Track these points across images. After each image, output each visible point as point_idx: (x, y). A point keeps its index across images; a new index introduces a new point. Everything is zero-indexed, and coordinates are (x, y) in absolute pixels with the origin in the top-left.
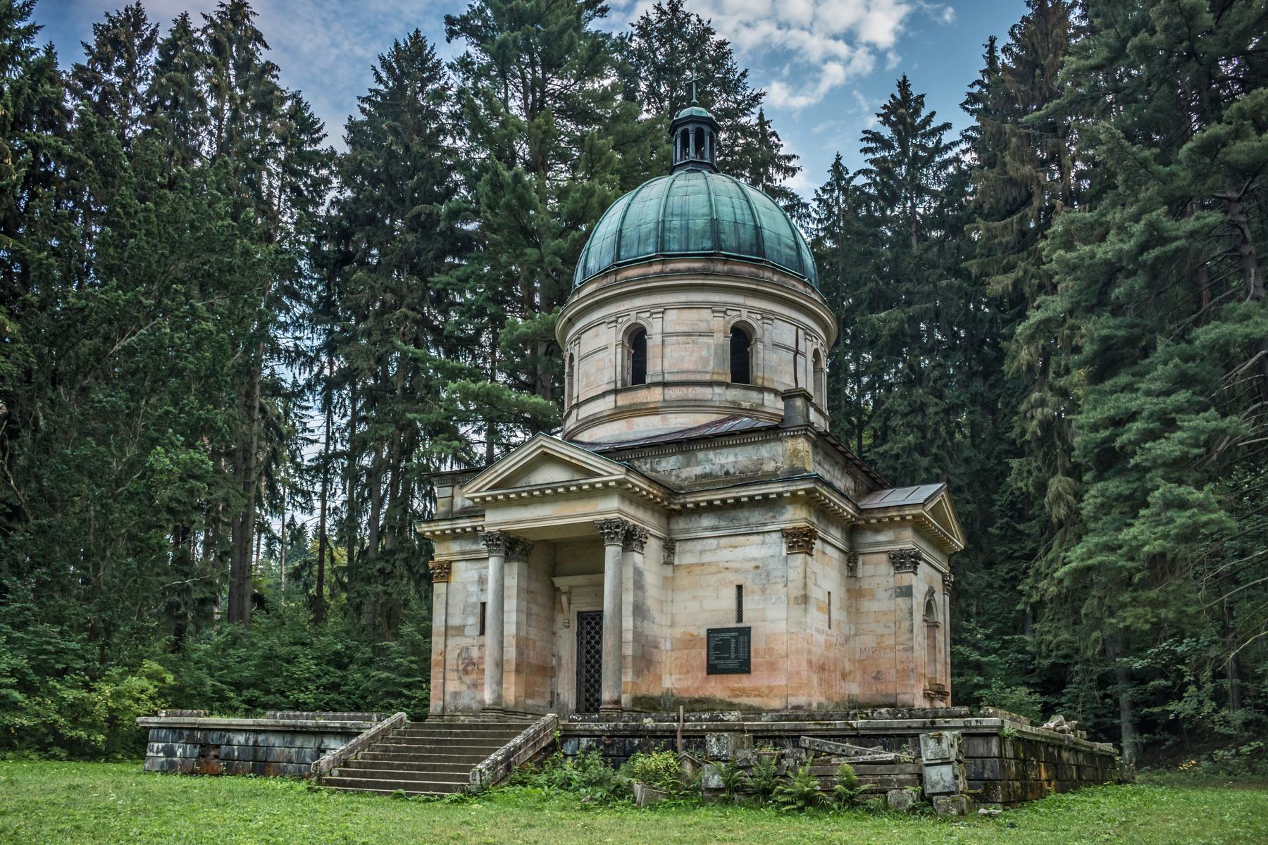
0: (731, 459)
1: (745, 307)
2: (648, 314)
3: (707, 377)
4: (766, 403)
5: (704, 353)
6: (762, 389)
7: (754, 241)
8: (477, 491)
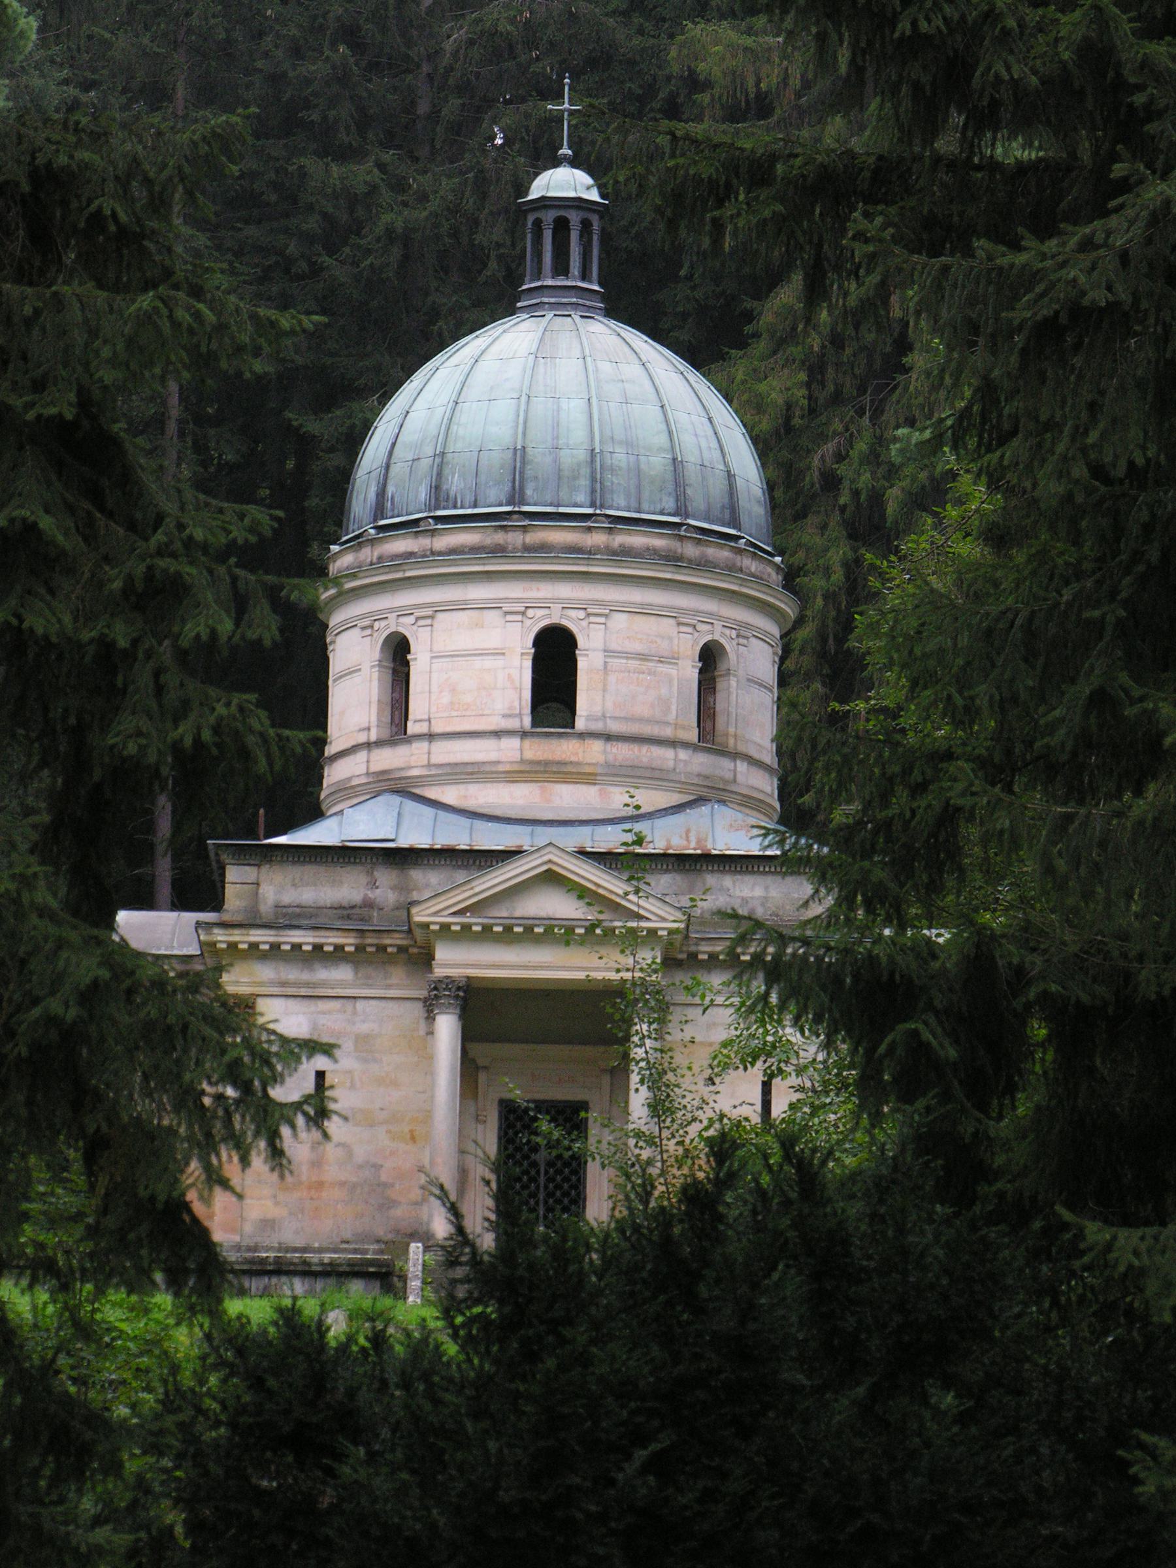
0: (758, 892)
1: (720, 618)
2: (582, 614)
3: (668, 732)
4: (740, 778)
5: (664, 691)
6: (735, 755)
7: (726, 500)
8: (436, 914)
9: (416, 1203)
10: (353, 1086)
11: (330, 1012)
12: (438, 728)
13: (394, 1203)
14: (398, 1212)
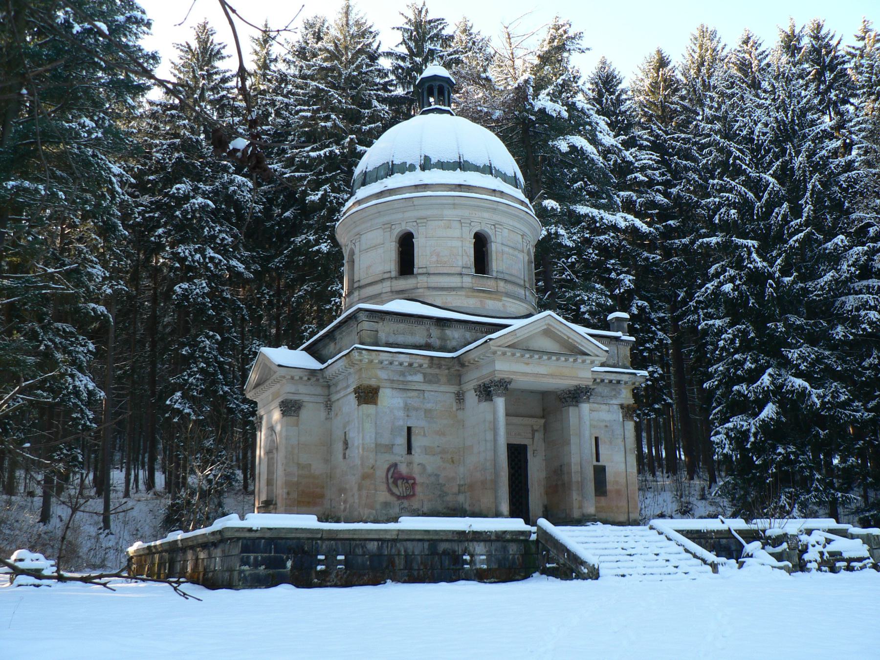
9: (455, 494)
10: (425, 435)
11: (412, 397)
12: (432, 271)
13: (447, 494)
14: (448, 498)
